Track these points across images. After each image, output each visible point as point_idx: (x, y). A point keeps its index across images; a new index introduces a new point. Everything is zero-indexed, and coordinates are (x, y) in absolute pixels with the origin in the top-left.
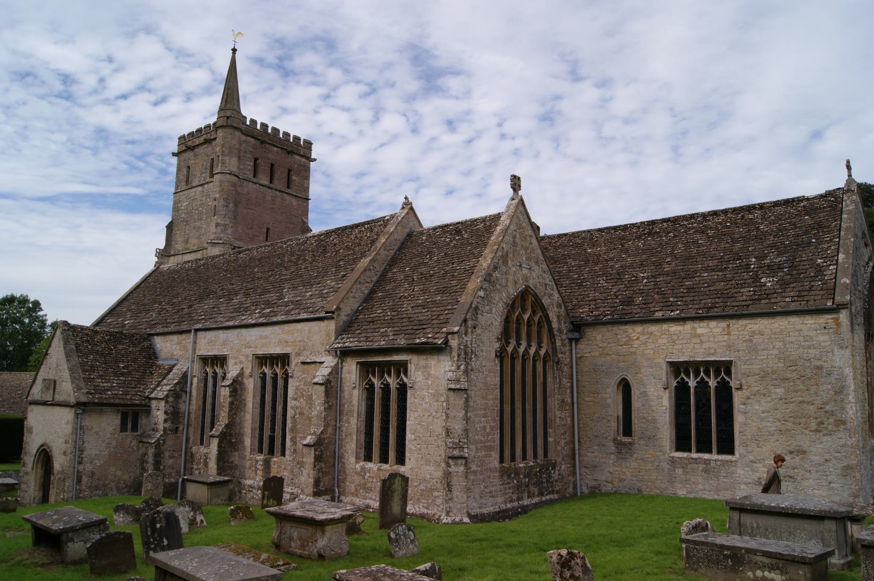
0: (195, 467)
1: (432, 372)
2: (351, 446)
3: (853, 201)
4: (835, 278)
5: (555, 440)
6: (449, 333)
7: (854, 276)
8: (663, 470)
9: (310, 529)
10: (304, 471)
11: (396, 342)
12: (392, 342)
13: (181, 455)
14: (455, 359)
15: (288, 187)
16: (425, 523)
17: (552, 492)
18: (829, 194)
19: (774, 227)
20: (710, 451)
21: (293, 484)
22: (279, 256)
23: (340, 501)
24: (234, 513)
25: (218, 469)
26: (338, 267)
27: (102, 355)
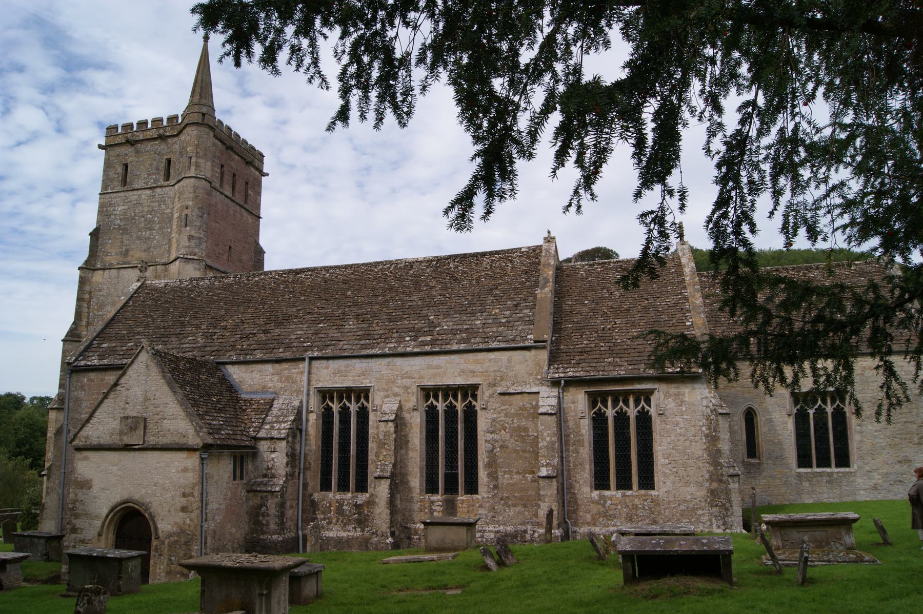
1: (687, 399)
10: (542, 505)
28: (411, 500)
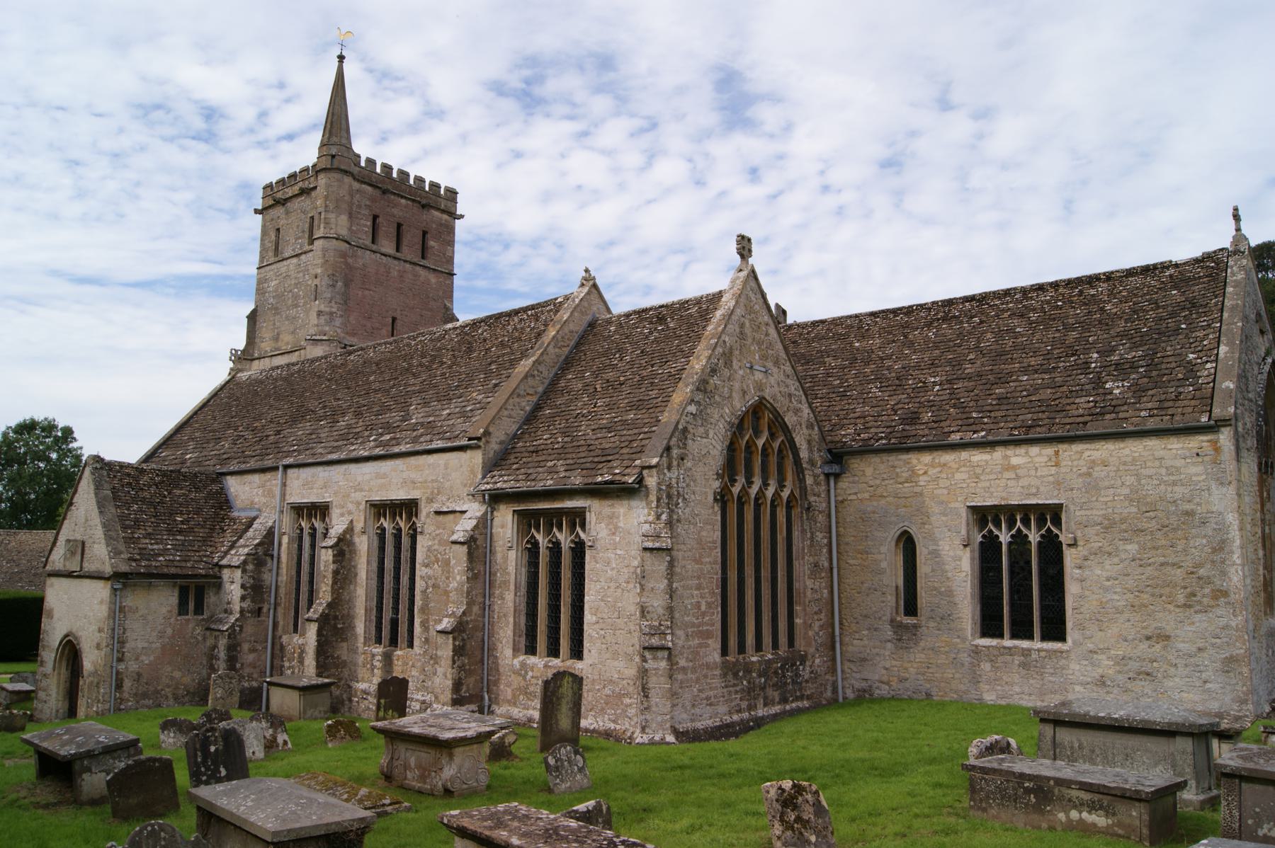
0: (287, 664)
1: (621, 524)
2: (506, 633)
3: (1242, 268)
4: (1214, 381)
5: (805, 622)
6: (644, 468)
7: (1243, 378)
8: (963, 665)
9: (433, 752)
11: (569, 481)
12: (563, 481)
13: (266, 648)
14: (654, 505)
15: (423, 257)
16: (603, 742)
17: (801, 698)
18: (1207, 257)
19: (1126, 307)
20: (1030, 637)
21: (426, 689)
22: (404, 358)
23: (491, 712)
24: (332, 731)
25: (318, 667)
26: (489, 374)
27: (151, 503)
28: (355, 651)
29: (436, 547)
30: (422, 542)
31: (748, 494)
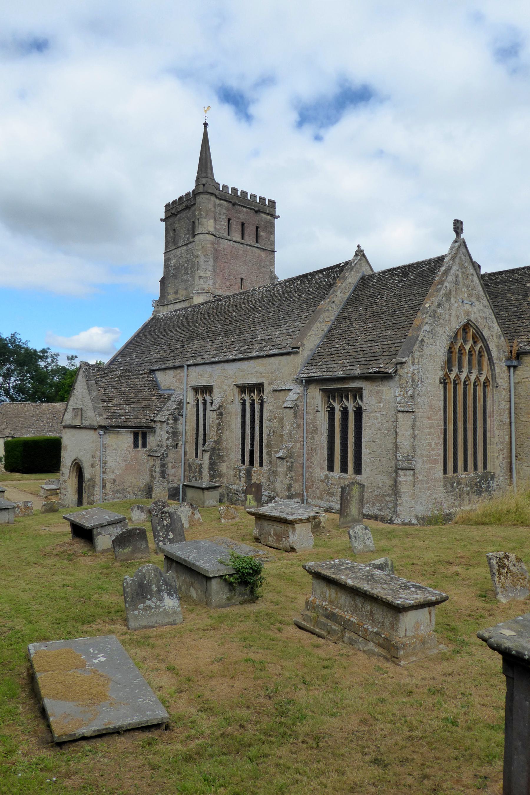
6: (397, 364)
15: (257, 242)
29: (275, 410)
30: (266, 408)
31: (459, 378)
